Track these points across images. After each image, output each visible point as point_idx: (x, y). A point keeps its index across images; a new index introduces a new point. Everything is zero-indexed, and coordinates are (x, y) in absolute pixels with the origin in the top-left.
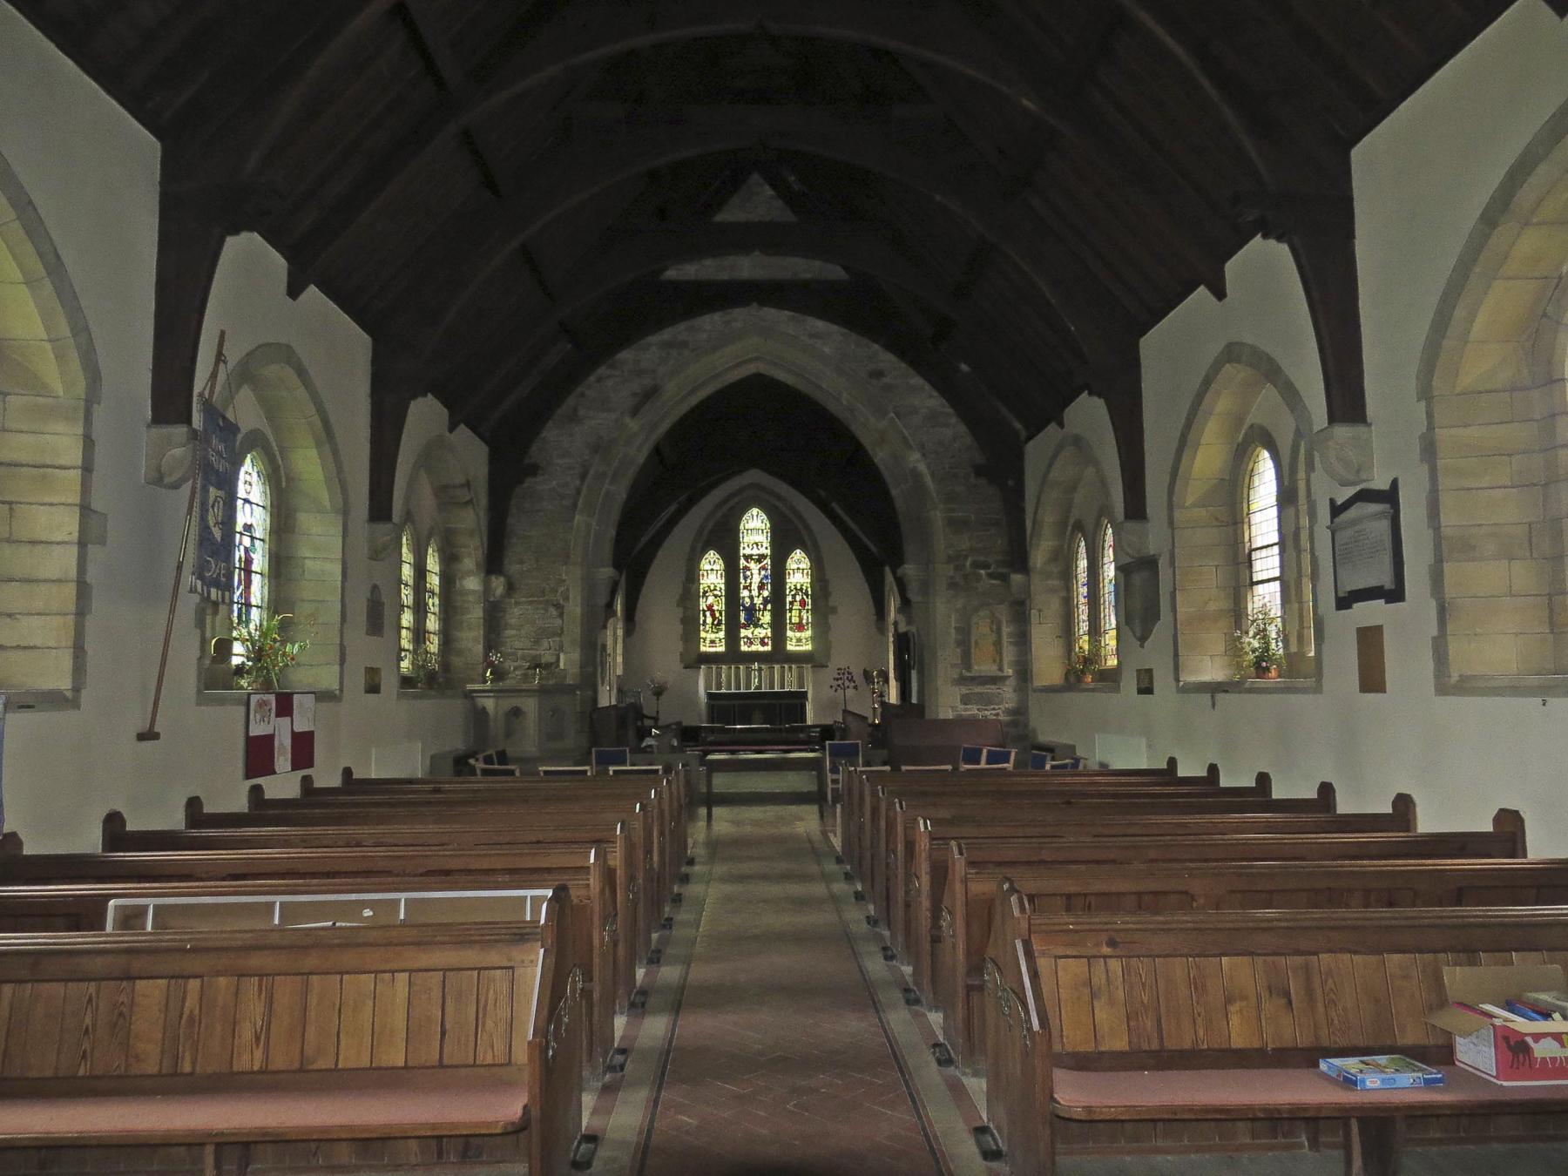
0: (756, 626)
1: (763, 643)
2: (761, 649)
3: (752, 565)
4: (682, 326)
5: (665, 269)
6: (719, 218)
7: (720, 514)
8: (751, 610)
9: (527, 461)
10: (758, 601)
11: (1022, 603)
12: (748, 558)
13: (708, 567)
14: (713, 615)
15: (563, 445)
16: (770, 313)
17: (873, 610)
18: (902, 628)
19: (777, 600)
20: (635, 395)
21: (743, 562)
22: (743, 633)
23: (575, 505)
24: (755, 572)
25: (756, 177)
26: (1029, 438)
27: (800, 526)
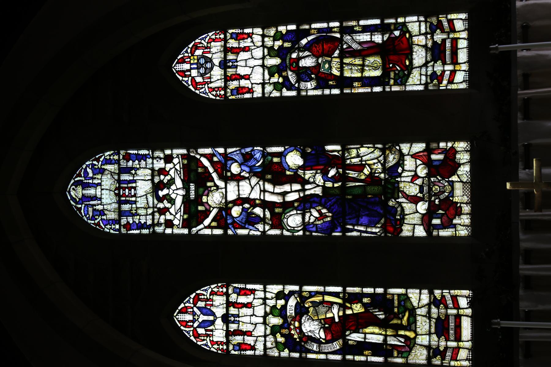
8: (344, 203)
12: (194, 212)
13: (219, 335)
14: (359, 322)
21: (206, 229)
22: (413, 228)
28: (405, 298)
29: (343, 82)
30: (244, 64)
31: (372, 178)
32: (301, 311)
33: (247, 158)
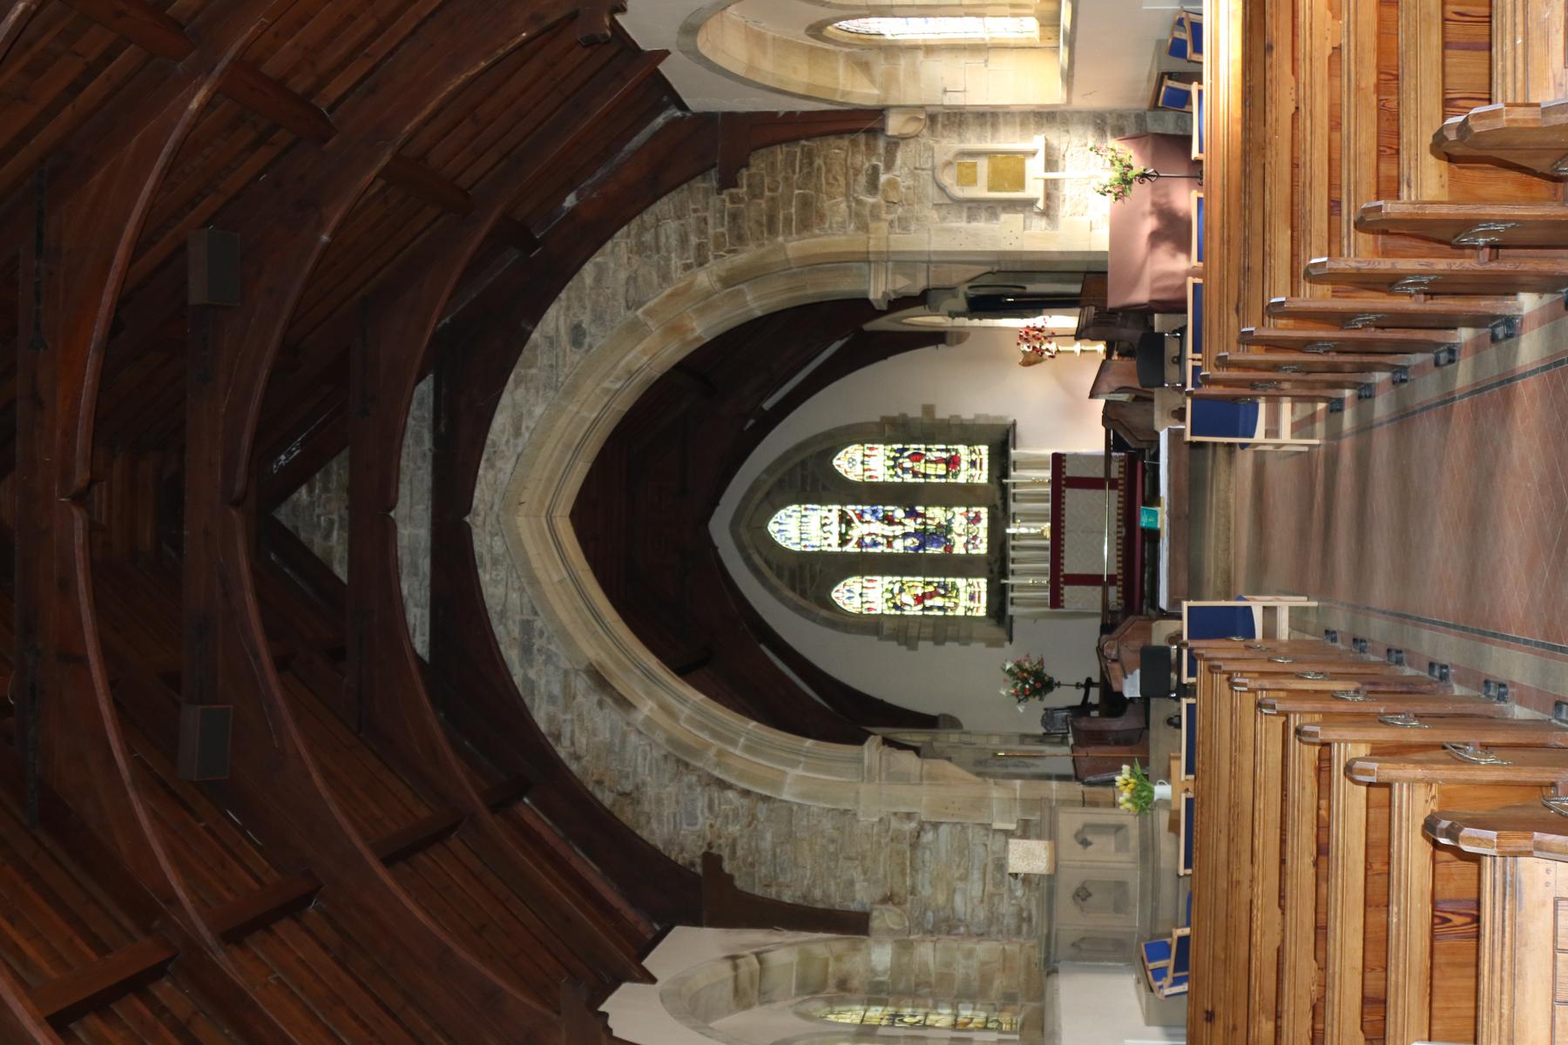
0: (949, 529)
1: (977, 519)
2: (984, 523)
3: (858, 531)
4: (499, 630)
5: (418, 658)
6: (341, 571)
7: (774, 580)
9: (699, 870)
10: (911, 525)
11: (932, 118)
12: (844, 540)
13: (857, 601)
14: (931, 596)
15: (674, 821)
16: (481, 494)
17: (929, 351)
18: (961, 304)
19: (908, 496)
20: (601, 704)
21: (851, 548)
22: (959, 549)
23: (766, 799)
24: (865, 529)
25: (283, 514)
26: (682, 106)
27: (798, 459)
28: (954, 585)
29: (925, 476)
30: (861, 462)
31: (939, 525)
32: (901, 590)
33: (874, 512)
